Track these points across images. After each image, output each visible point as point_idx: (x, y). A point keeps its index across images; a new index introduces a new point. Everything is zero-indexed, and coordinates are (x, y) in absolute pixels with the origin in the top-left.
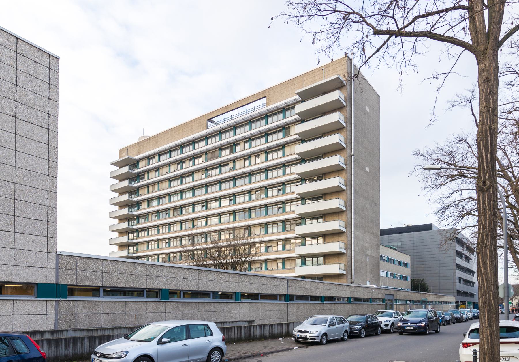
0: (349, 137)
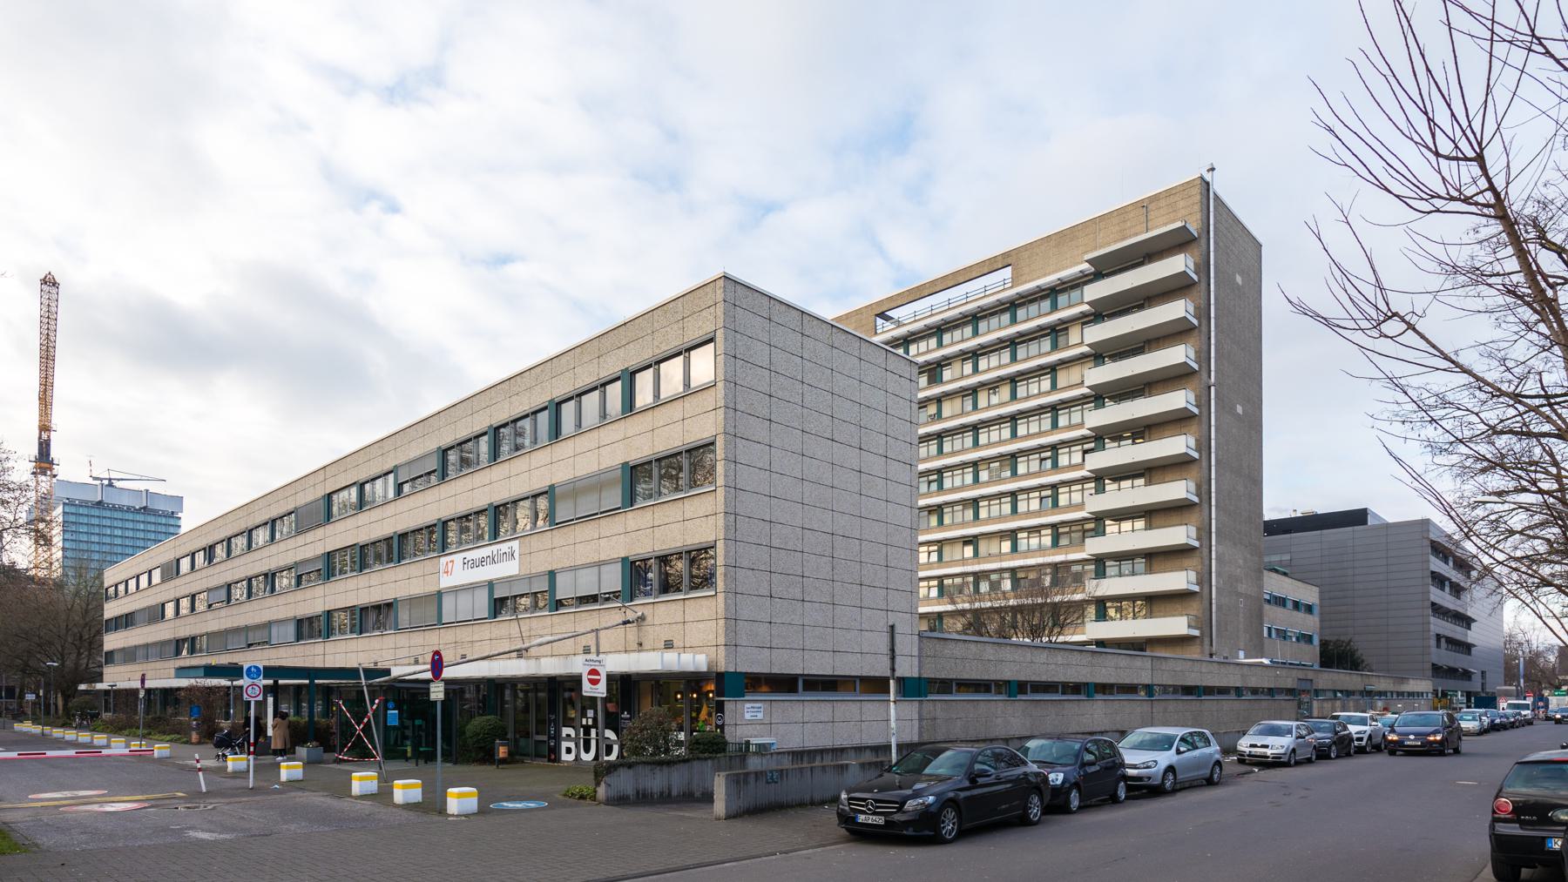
0: (1205, 347)
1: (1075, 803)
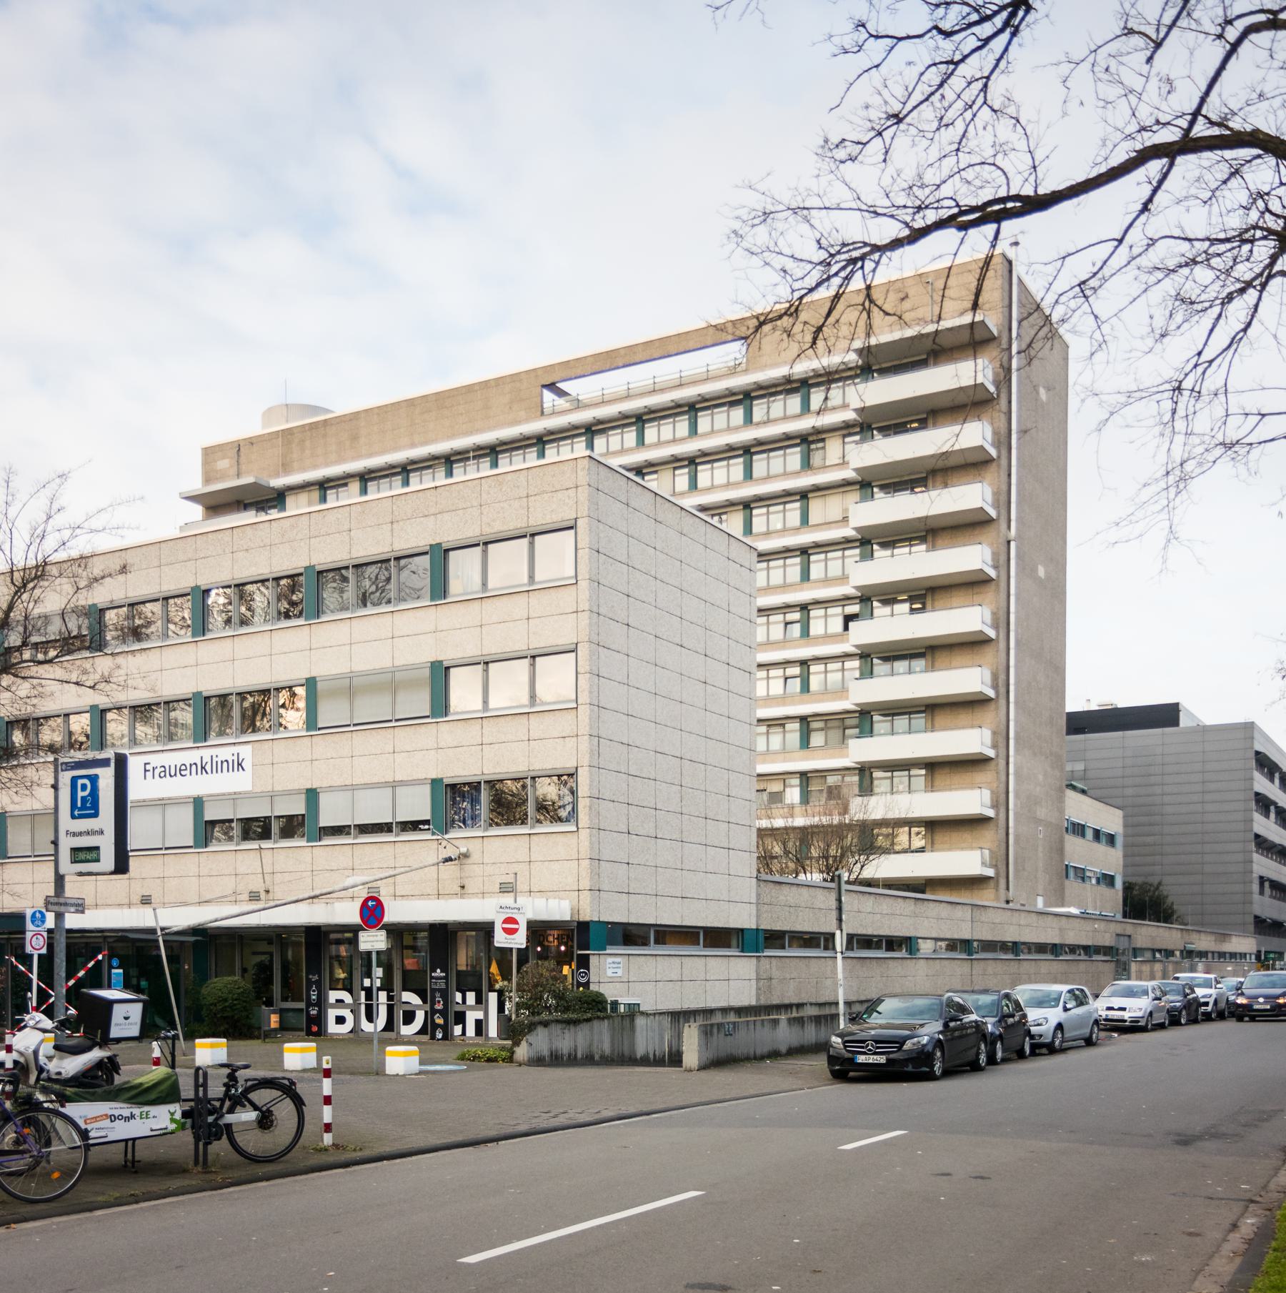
0: (1004, 487)
1: (938, 1068)
